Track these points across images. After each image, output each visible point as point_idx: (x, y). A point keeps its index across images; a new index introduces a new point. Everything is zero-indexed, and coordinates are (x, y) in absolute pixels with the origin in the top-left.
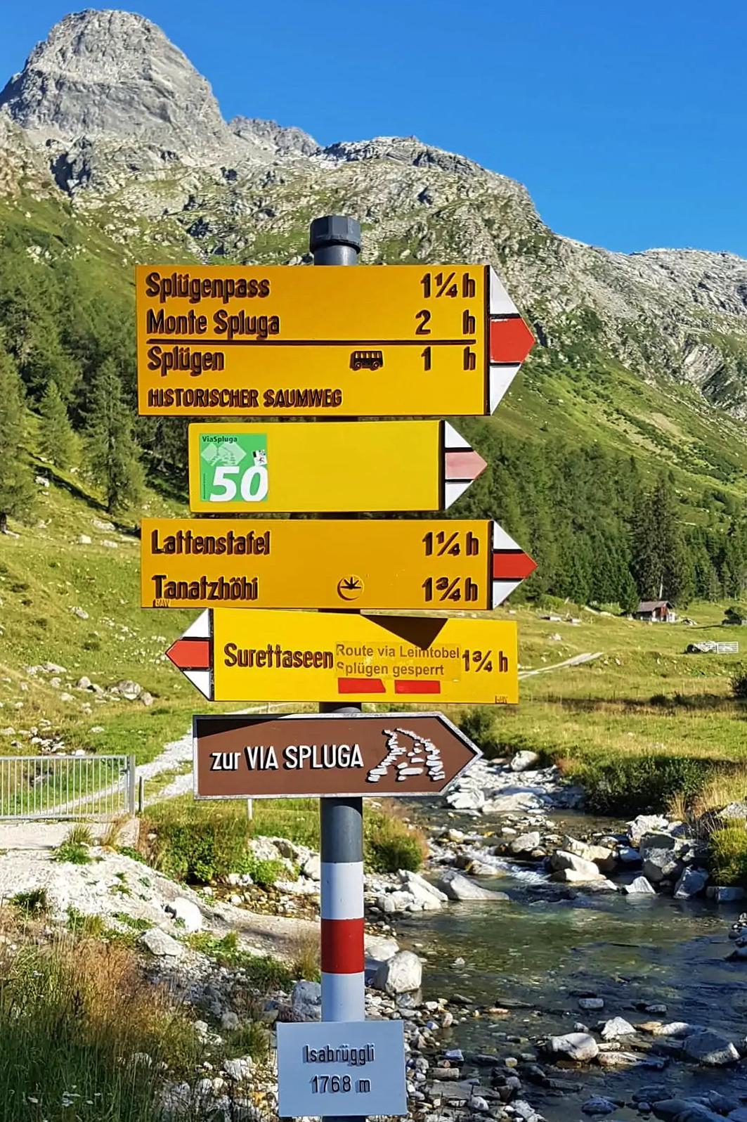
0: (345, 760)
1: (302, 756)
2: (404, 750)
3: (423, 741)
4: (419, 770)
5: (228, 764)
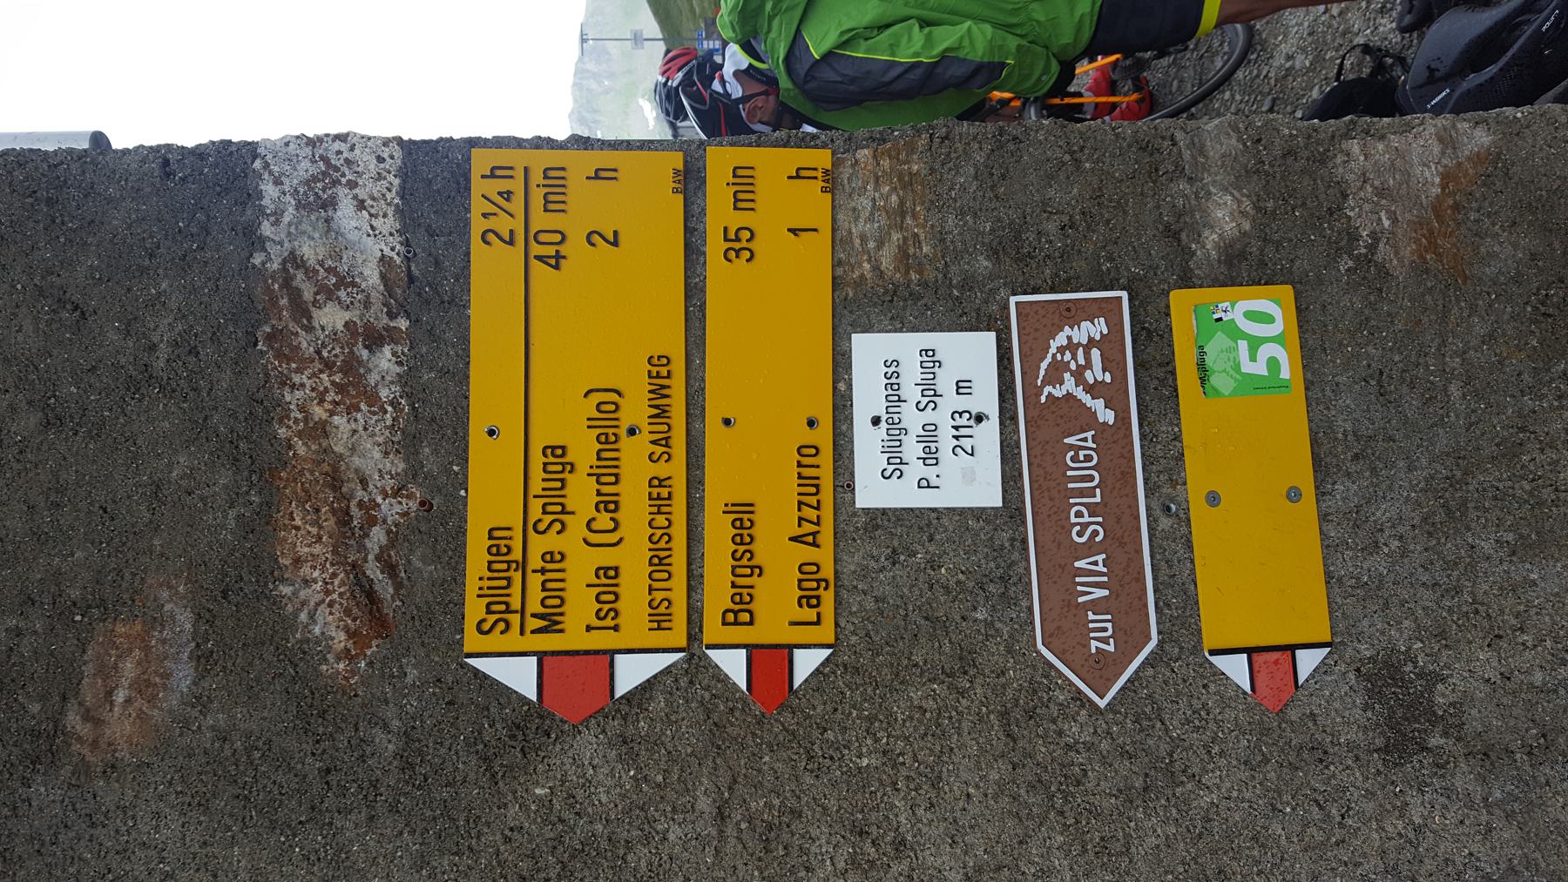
0: (1088, 458)
1: (1086, 519)
2: (1067, 376)
3: (1053, 350)
4: (1096, 354)
5: (1105, 630)
